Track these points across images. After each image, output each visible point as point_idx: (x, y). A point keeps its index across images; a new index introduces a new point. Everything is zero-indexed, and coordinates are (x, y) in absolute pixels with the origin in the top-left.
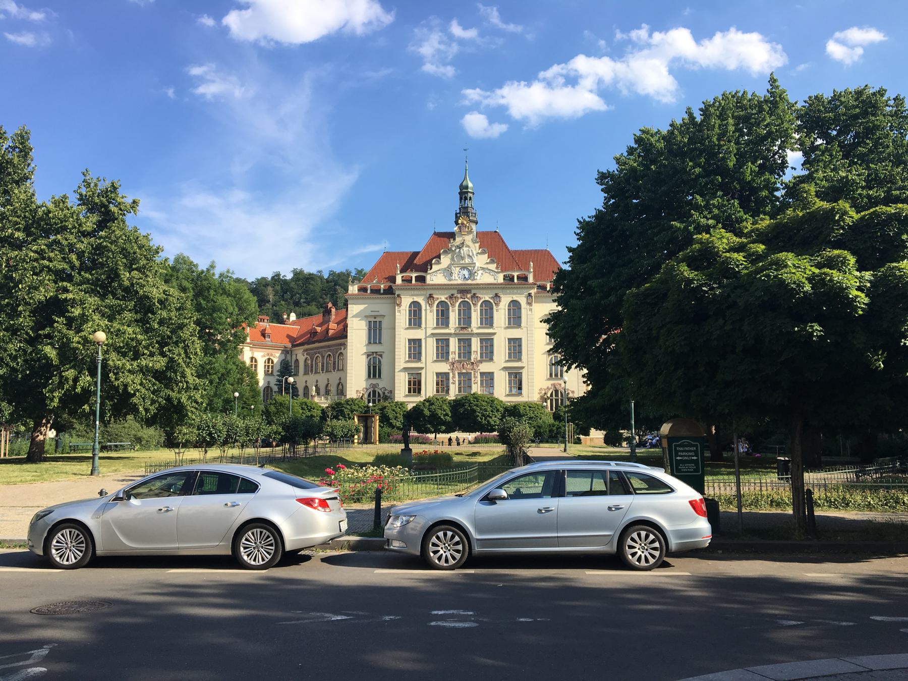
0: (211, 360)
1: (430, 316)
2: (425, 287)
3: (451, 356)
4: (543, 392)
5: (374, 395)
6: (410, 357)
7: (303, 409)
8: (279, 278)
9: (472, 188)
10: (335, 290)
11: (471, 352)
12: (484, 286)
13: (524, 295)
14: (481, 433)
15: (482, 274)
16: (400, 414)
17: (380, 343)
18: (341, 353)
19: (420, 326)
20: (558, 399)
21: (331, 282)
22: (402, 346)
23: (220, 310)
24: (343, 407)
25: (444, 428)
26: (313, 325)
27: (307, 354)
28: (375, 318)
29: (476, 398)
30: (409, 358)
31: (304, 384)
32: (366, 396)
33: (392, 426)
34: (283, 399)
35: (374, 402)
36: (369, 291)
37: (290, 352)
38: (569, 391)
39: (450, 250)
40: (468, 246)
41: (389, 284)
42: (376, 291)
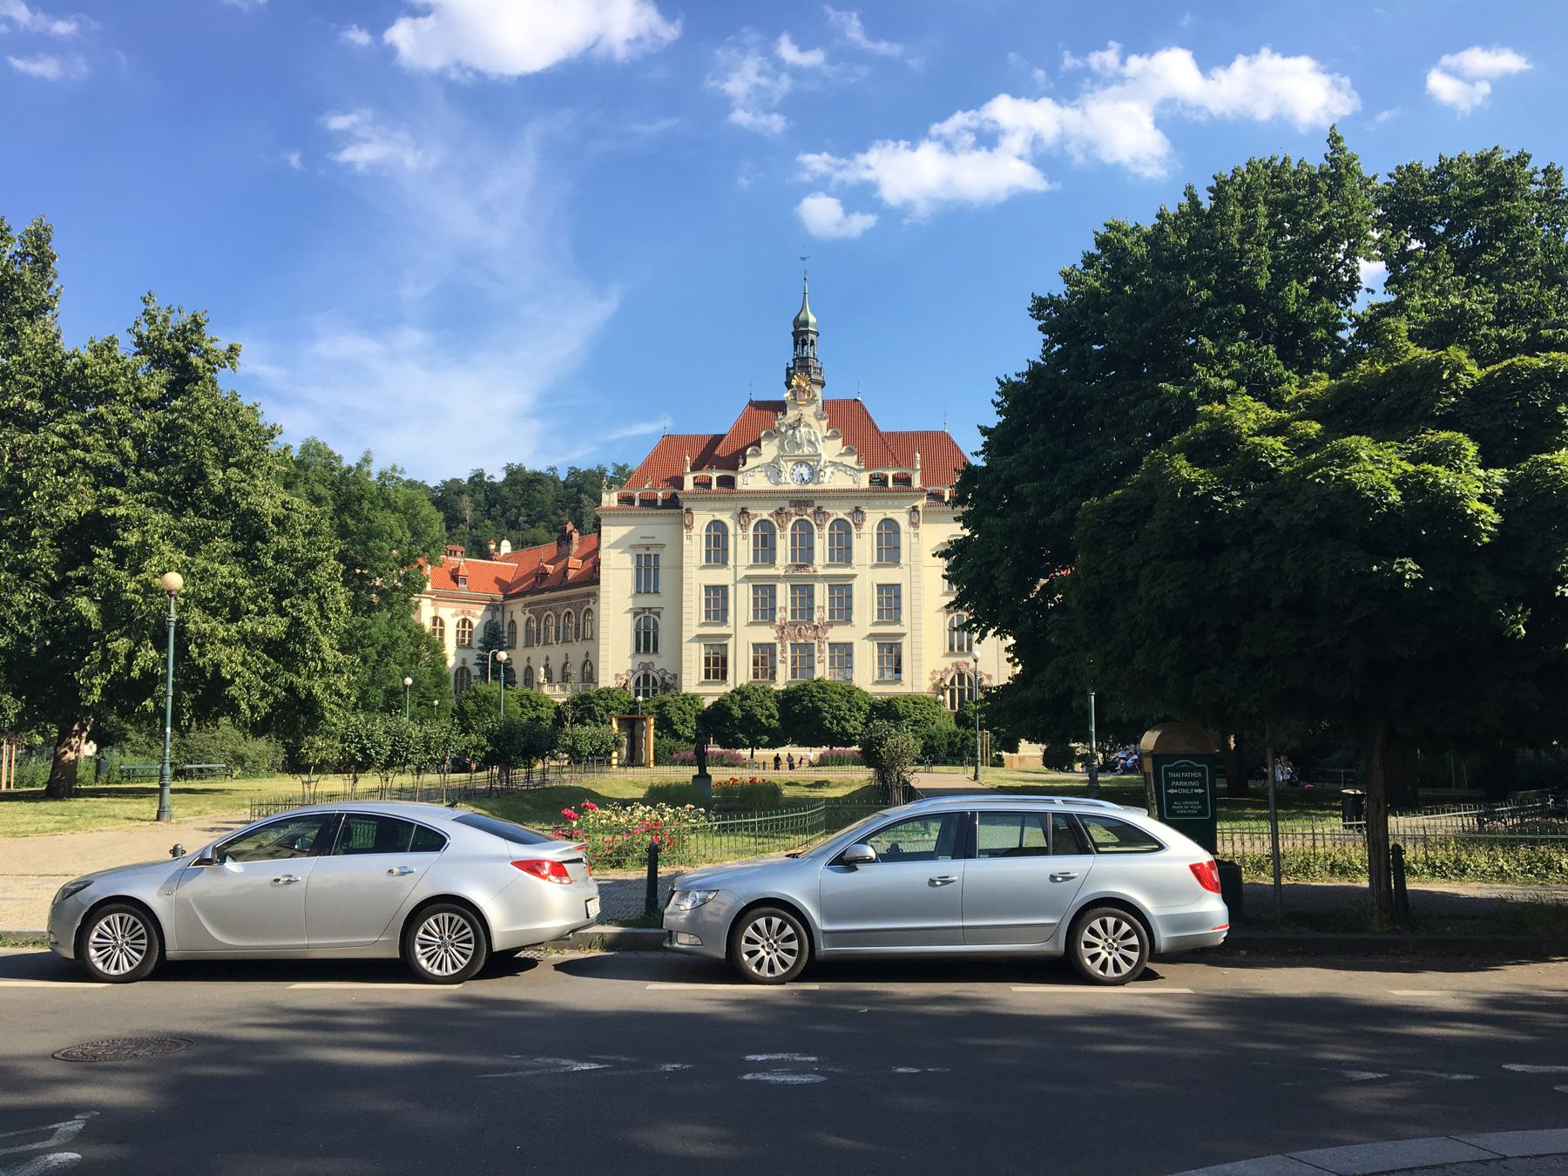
0: (365, 622)
1: (742, 546)
2: (734, 496)
3: (779, 616)
4: (938, 677)
5: (646, 682)
6: (707, 616)
7: (522, 706)
8: (482, 481)
9: (815, 325)
10: (579, 501)
11: (813, 608)
13: (904, 510)
15: (832, 473)
16: (691, 715)
17: (656, 592)
19: (725, 563)
20: (964, 690)
21: (572, 487)
22: (695, 598)
25: (766, 738)
27: (530, 612)
28: (648, 549)
29: (822, 688)
30: (706, 619)
32: (632, 684)
33: (676, 736)
34: (489, 689)
35: (646, 694)
36: (637, 503)
37: (500, 608)
38: (983, 676)
39: (777, 431)
40: (809, 426)
41: (672, 490)
42: (649, 503)
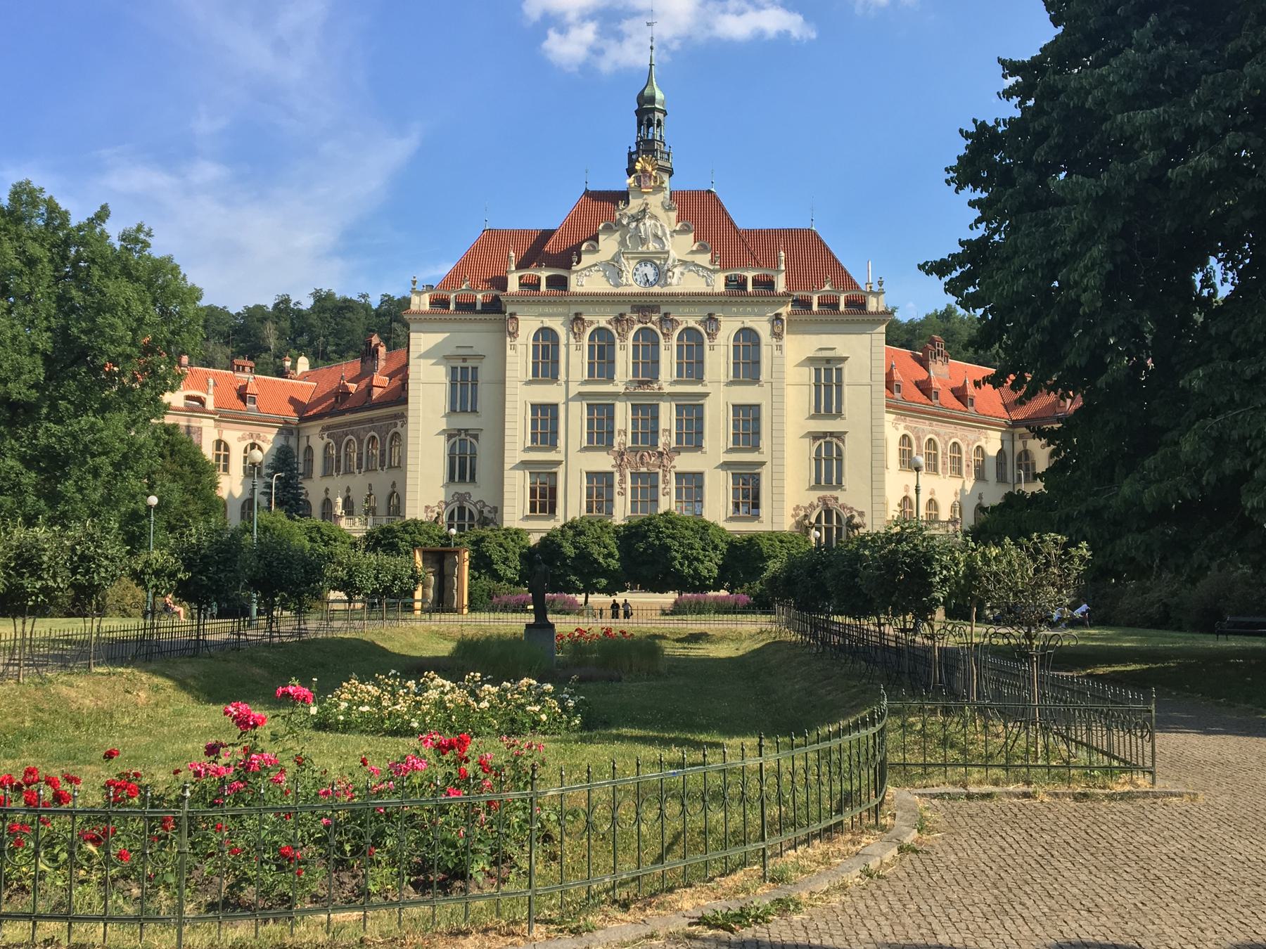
2: (568, 299)
4: (802, 513)
5: (462, 516)
7: (312, 540)
8: (288, 307)
9: (663, 103)
10: (391, 330)
11: (657, 432)
12: (686, 299)
14: (680, 594)
15: (682, 274)
16: (514, 553)
17: (474, 411)
18: (396, 433)
19: (554, 378)
20: (832, 528)
21: (384, 315)
23: (112, 309)
24: (396, 537)
25: (604, 582)
26: (342, 378)
28: (464, 360)
29: (671, 522)
31: (323, 496)
32: (445, 517)
33: (497, 577)
34: (272, 518)
35: (461, 528)
36: (452, 307)
37: (295, 433)
38: (854, 513)
39: (619, 223)
40: (654, 217)
42: (466, 307)
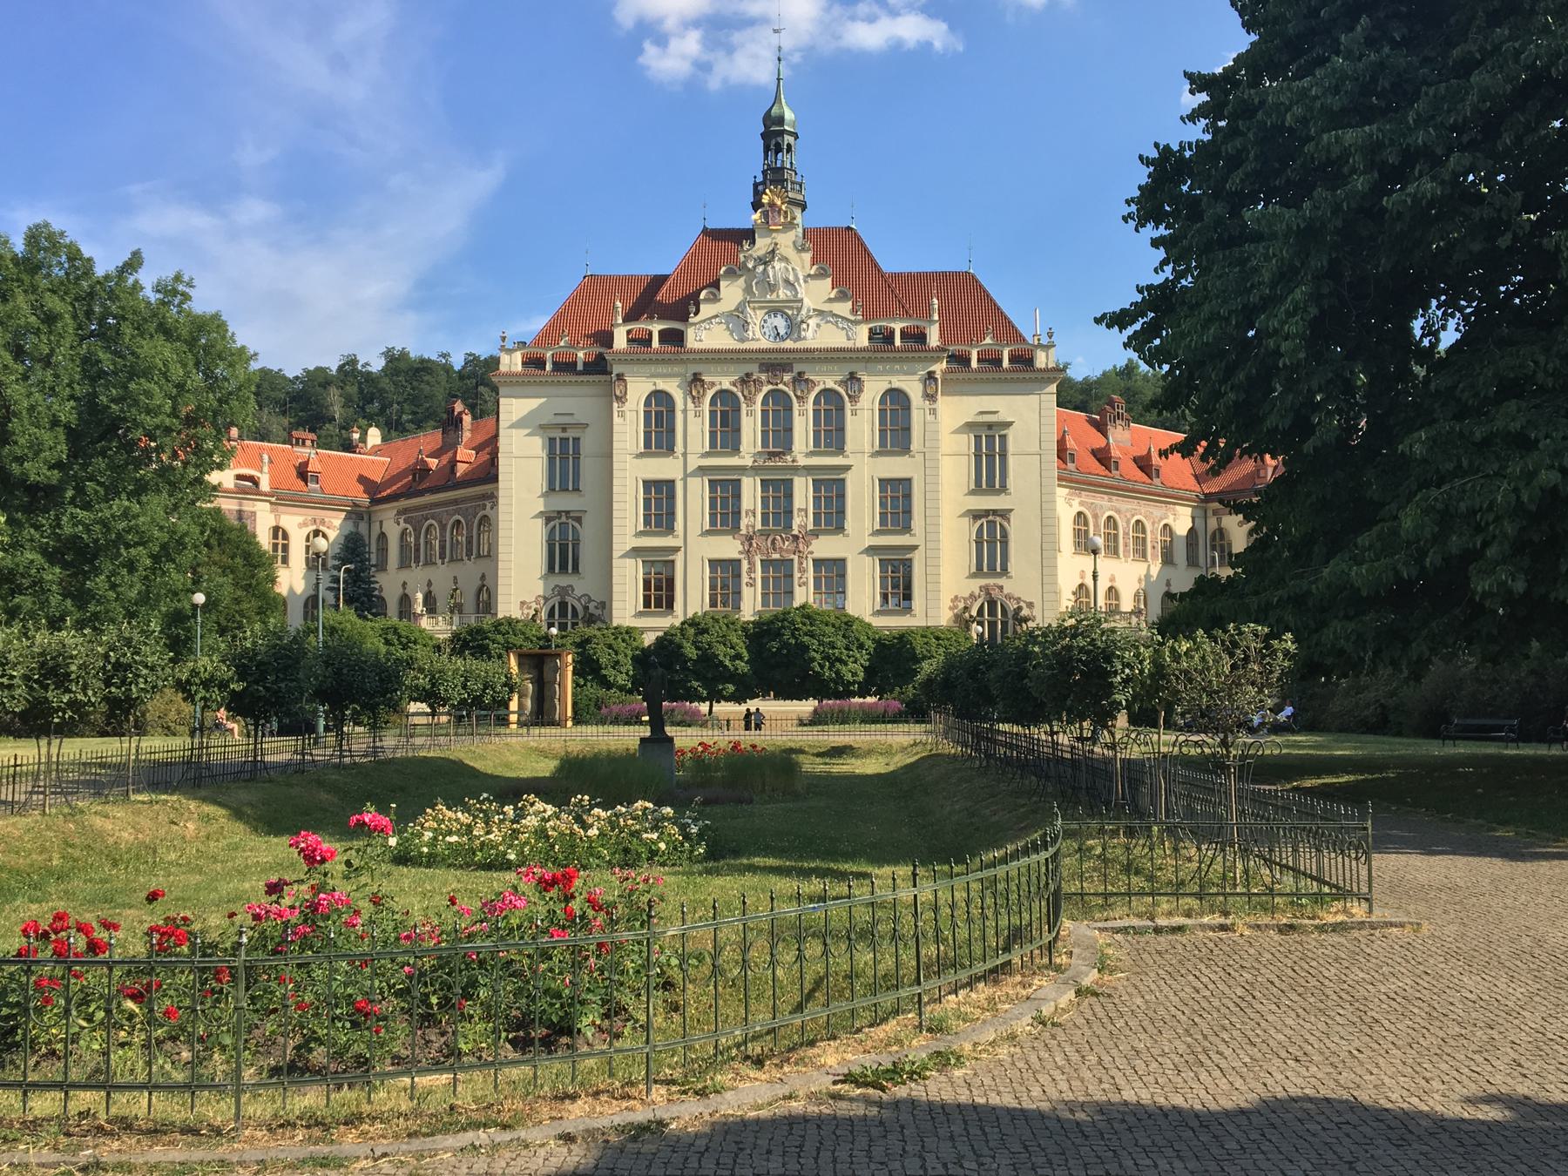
0: (128, 508)
1: (694, 427)
2: (684, 357)
3: (744, 522)
4: (961, 605)
5: (563, 614)
6: (647, 522)
7: (388, 642)
8: (355, 369)
9: (793, 124)
10: (477, 395)
11: (791, 512)
13: (917, 377)
15: (818, 326)
16: (626, 656)
17: (576, 489)
19: (671, 449)
20: (996, 623)
21: (469, 378)
22: (630, 499)
25: (731, 688)
27: (405, 521)
28: (564, 430)
29: (808, 617)
30: (645, 525)
32: (543, 615)
33: (606, 684)
34: (339, 618)
35: (562, 627)
36: (549, 367)
37: (366, 517)
38: (1022, 604)
39: (743, 267)
40: (785, 259)
41: (597, 349)
42: (565, 367)
